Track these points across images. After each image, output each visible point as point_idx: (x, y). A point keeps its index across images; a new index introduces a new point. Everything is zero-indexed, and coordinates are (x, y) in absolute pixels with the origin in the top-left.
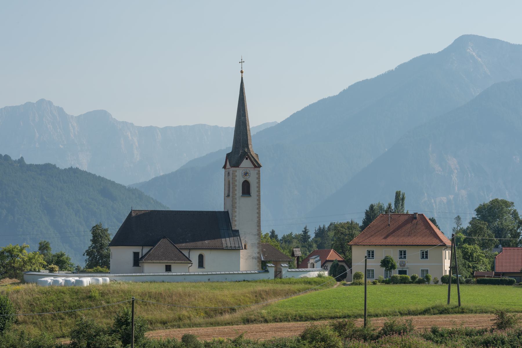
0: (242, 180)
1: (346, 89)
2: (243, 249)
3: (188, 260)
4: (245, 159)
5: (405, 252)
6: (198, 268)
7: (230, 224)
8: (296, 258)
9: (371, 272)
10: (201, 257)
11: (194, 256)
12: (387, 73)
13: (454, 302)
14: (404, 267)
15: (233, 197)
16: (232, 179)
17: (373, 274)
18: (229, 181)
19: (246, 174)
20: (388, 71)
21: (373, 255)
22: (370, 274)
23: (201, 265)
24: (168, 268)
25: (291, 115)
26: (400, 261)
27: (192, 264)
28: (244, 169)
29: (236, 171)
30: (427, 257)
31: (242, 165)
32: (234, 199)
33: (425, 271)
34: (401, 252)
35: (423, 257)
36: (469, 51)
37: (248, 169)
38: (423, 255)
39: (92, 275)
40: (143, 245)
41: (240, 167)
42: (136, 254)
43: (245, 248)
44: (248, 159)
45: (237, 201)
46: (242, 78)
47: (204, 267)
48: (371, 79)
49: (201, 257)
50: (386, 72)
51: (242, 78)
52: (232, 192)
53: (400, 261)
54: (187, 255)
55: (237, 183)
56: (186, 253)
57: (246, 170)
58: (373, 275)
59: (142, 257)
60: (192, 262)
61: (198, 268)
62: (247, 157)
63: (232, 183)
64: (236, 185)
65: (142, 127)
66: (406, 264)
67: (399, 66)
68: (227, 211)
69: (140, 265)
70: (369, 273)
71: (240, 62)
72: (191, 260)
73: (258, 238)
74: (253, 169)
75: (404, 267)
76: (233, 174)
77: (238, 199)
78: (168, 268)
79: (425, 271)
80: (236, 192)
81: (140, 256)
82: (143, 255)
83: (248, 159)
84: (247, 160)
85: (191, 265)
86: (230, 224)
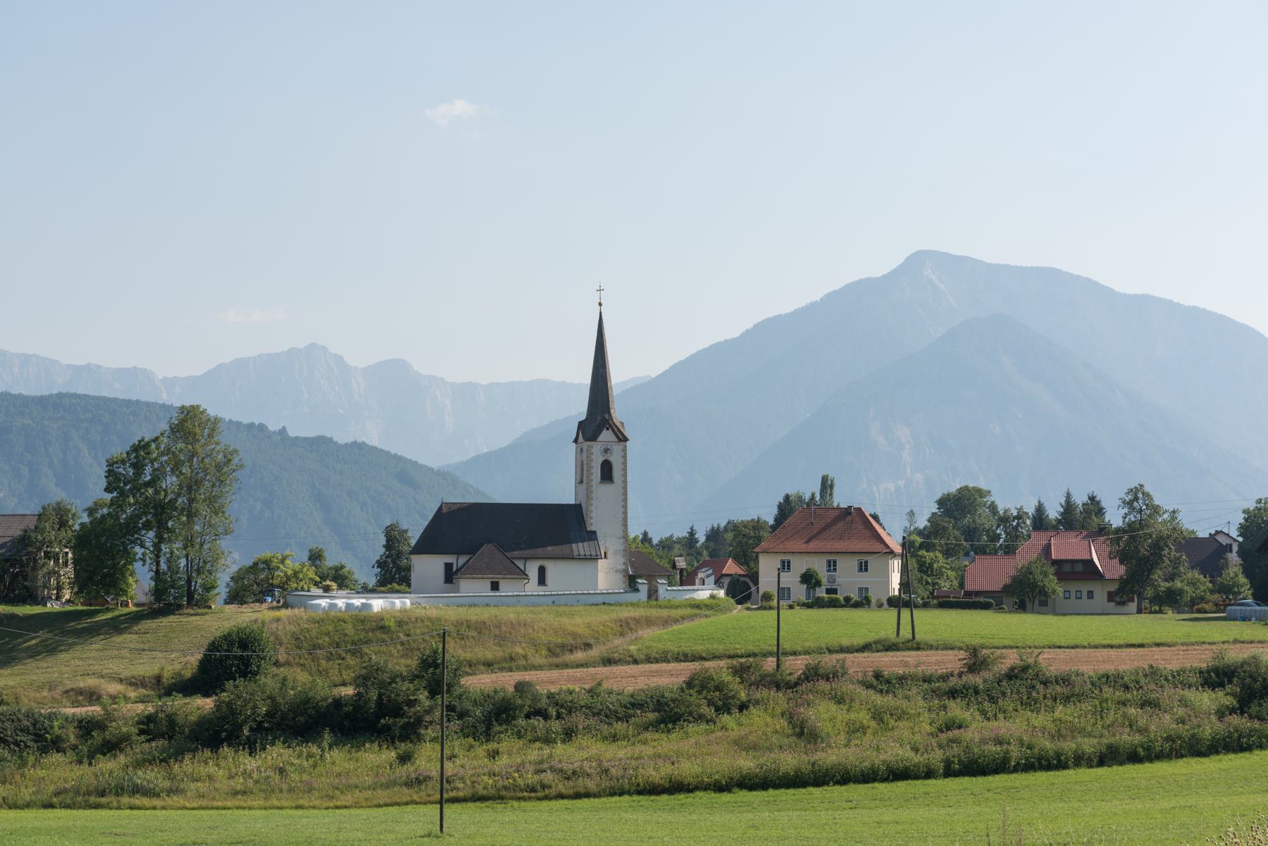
0: (601, 459)
2: (601, 558)
8: (678, 572)
10: (542, 571)
15: (587, 483)
16: (587, 457)
18: (582, 461)
21: (789, 566)
23: (542, 581)
24: (495, 586)
27: (529, 579)
29: (592, 447)
34: (783, 562)
35: (861, 569)
38: (861, 566)
40: (458, 553)
42: (448, 567)
45: (594, 489)
46: (601, 313)
49: (542, 571)
51: (601, 313)
56: (520, 564)
59: (458, 570)
63: (587, 464)
67: (826, 295)
69: (454, 581)
78: (495, 586)
81: (455, 569)
84: (608, 431)
85: (527, 581)
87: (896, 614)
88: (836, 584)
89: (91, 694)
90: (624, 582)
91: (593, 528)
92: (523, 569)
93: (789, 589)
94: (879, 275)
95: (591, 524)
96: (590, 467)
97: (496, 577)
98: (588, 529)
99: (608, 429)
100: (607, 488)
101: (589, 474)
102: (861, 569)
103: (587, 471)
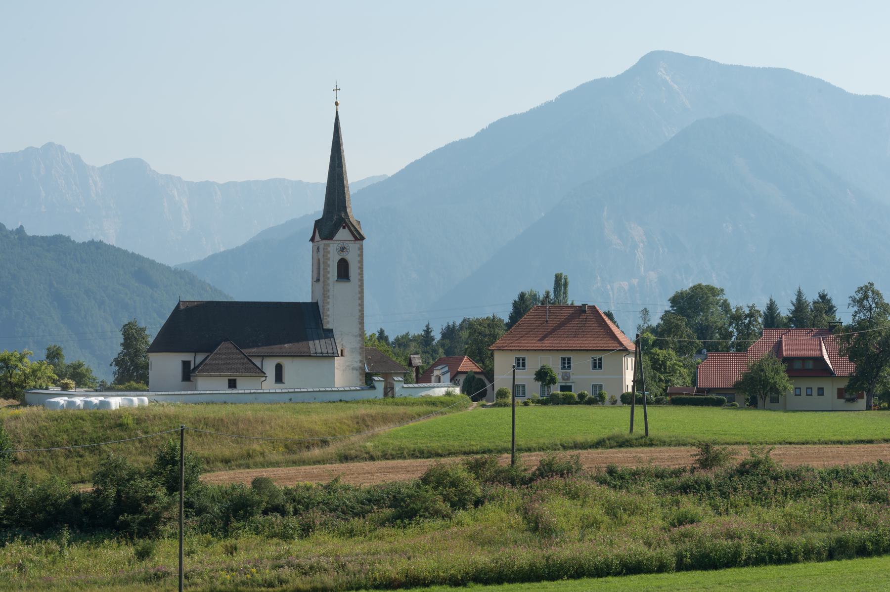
0: (337, 258)
1: (485, 128)
2: (338, 356)
4: (342, 228)
5: (569, 359)
9: (521, 389)
10: (279, 369)
15: (324, 282)
16: (324, 255)
17: (525, 391)
19: (343, 249)
21: (524, 363)
23: (279, 378)
24: (232, 384)
26: (563, 373)
27: (266, 377)
28: (340, 242)
29: (328, 245)
30: (600, 367)
33: (521, 386)
34: (564, 359)
35: (595, 367)
36: (661, 73)
37: (346, 242)
40: (196, 351)
41: (315, 241)
42: (186, 364)
44: (346, 227)
45: (331, 287)
46: (337, 112)
48: (521, 114)
49: (279, 369)
50: (542, 104)
51: (337, 112)
52: (324, 276)
53: (563, 373)
56: (257, 362)
60: (266, 375)
62: (344, 225)
66: (571, 377)
68: (316, 301)
69: (192, 379)
73: (360, 340)
74: (353, 242)
76: (324, 249)
78: (232, 384)
79: (521, 386)
81: (192, 367)
82: (196, 365)
83: (346, 227)
85: (264, 378)
86: (320, 321)
91: (329, 326)
95: (328, 322)
96: (327, 266)
97: (232, 375)
98: (325, 327)
100: (343, 286)
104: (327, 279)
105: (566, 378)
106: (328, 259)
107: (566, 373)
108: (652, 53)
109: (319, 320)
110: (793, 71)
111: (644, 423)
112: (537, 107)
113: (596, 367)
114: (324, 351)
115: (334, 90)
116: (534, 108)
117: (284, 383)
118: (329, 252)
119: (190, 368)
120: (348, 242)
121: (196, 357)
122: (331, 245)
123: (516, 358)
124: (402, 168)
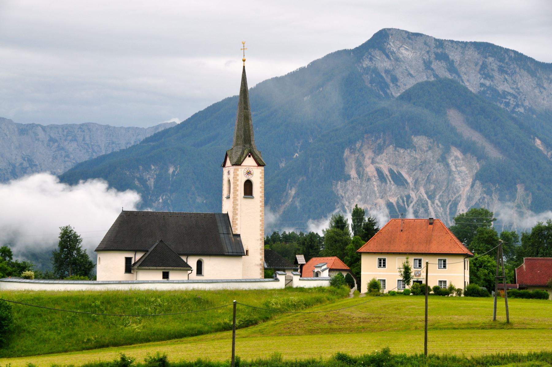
0: (245, 179)
1: (253, 87)
2: (245, 255)
3: (186, 267)
4: (248, 156)
5: (384, 260)
6: (197, 276)
7: (230, 228)
8: (299, 266)
9: (443, 284)
10: (199, 264)
11: (192, 262)
12: (298, 70)
13: (501, 317)
14: (419, 278)
15: (234, 198)
16: (234, 178)
17: (385, 284)
18: (229, 181)
19: (249, 173)
20: (299, 68)
21: (384, 263)
22: (442, 285)
23: (199, 271)
24: (166, 276)
25: (192, 115)
26: (415, 271)
27: (192, 271)
28: (246, 167)
29: (238, 170)
30: (384, 266)
31: (244, 163)
32: (235, 199)
33: (443, 282)
34: (380, 260)
35: (380, 266)
36: (390, 46)
37: (251, 167)
38: (380, 263)
39: (19, 281)
40: (136, 251)
41: (226, 166)
42: (128, 260)
43: (247, 254)
44: (251, 156)
45: (239, 202)
46: (244, 67)
47: (202, 274)
48: (281, 77)
49: (199, 264)
50: (297, 69)
51: (244, 67)
52: (234, 193)
53: (415, 271)
54: (185, 260)
55: (238, 183)
56: (184, 258)
57: (249, 169)
58: (385, 286)
59: (135, 263)
60: (192, 269)
61: (197, 276)
62: (250, 154)
63: (234, 183)
64: (238, 185)
65: (22, 124)
66: (422, 274)
67: (312, 63)
68: (227, 213)
69: (132, 272)
70: (384, 283)
71: (241, 49)
72: (447, 265)
73: (260, 243)
74: (256, 167)
75: (419, 278)
76: (234, 172)
77: (239, 200)
78: (166, 276)
79: (443, 282)
80: (237, 193)
81: (133, 262)
82: (136, 261)
83: (251, 156)
84: (249, 158)
85: (190, 272)
86: (230, 228)
87: (424, 300)
88: (421, 277)
89: (492, 357)
90: (261, 274)
91: (237, 232)
92: (186, 261)
93: (384, 281)
94: (353, 48)
95: (237, 229)
96: (236, 185)
97: (166, 269)
98: (234, 233)
99: (249, 156)
100: (248, 201)
101: (236, 190)
102: (380, 266)
103: (234, 188)
104: (235, 196)
105: (418, 275)
106: (237, 180)
107: (418, 272)
108: (384, 30)
109: (230, 227)
110: (327, 55)
111: (497, 312)
112: (294, 72)
113: (441, 267)
114: (230, 250)
115: (241, 49)
116: (291, 72)
117: (203, 276)
118: (238, 175)
119: (131, 263)
120: (252, 168)
121: (136, 256)
122: (240, 170)
123: (378, 259)
124: (188, 117)
